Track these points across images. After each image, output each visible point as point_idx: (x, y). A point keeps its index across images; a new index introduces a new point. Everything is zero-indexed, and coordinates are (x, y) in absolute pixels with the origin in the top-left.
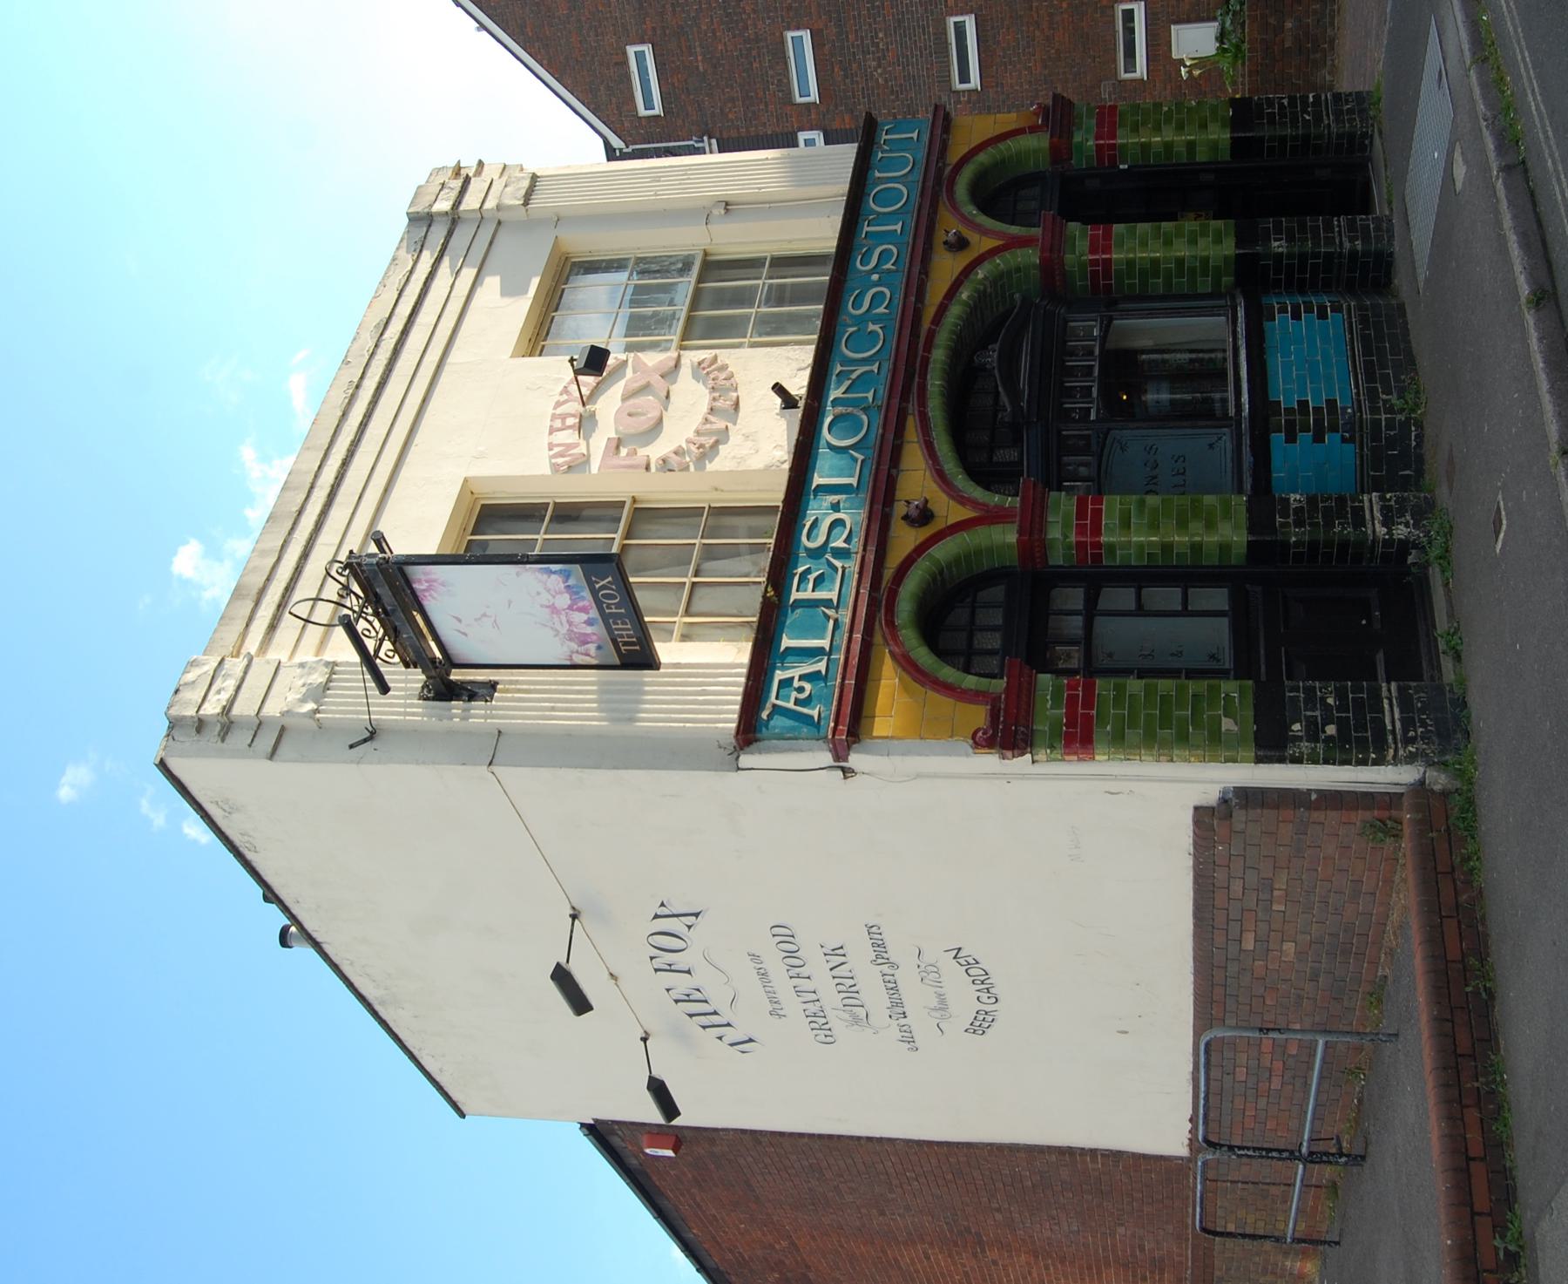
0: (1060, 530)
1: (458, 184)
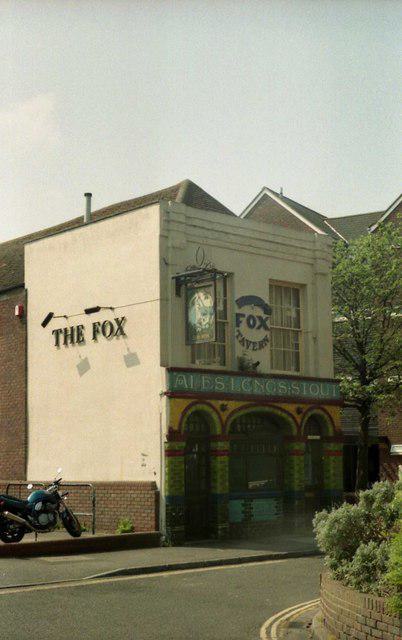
0: (221, 445)
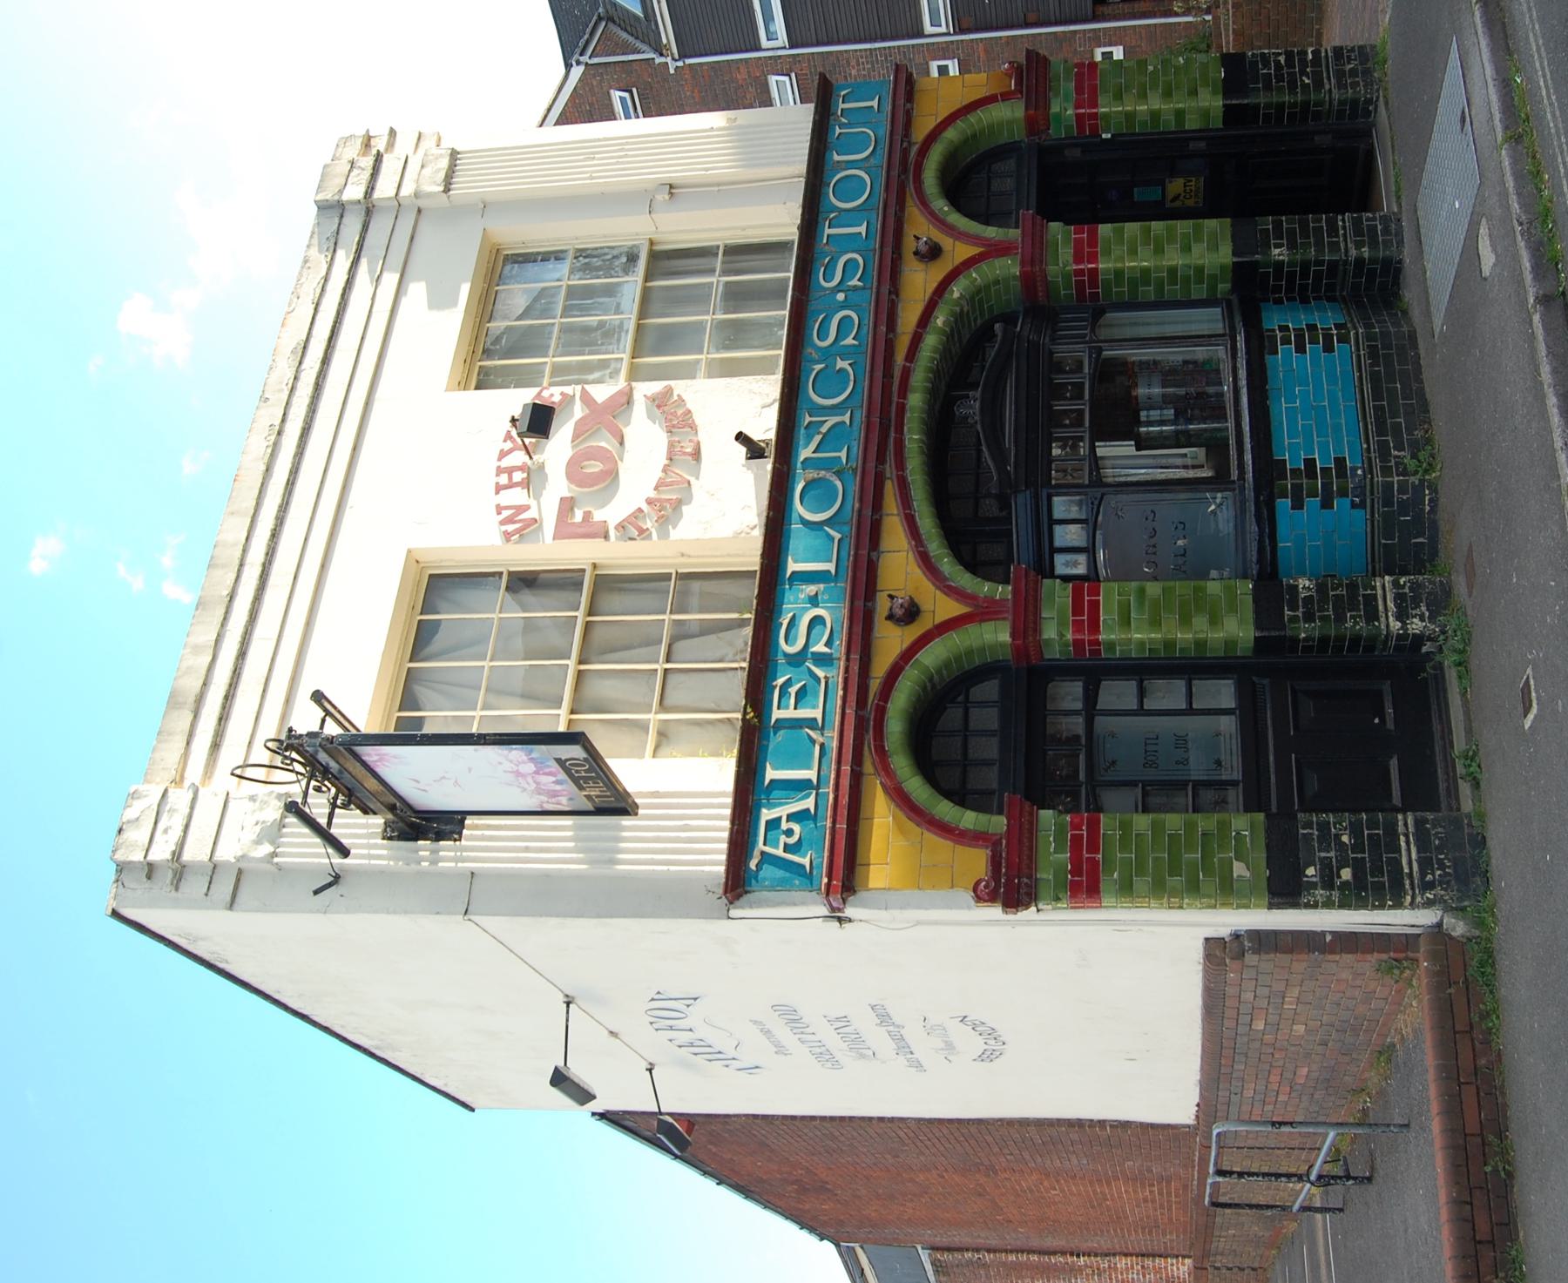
0: (1056, 632)
1: (368, 162)
